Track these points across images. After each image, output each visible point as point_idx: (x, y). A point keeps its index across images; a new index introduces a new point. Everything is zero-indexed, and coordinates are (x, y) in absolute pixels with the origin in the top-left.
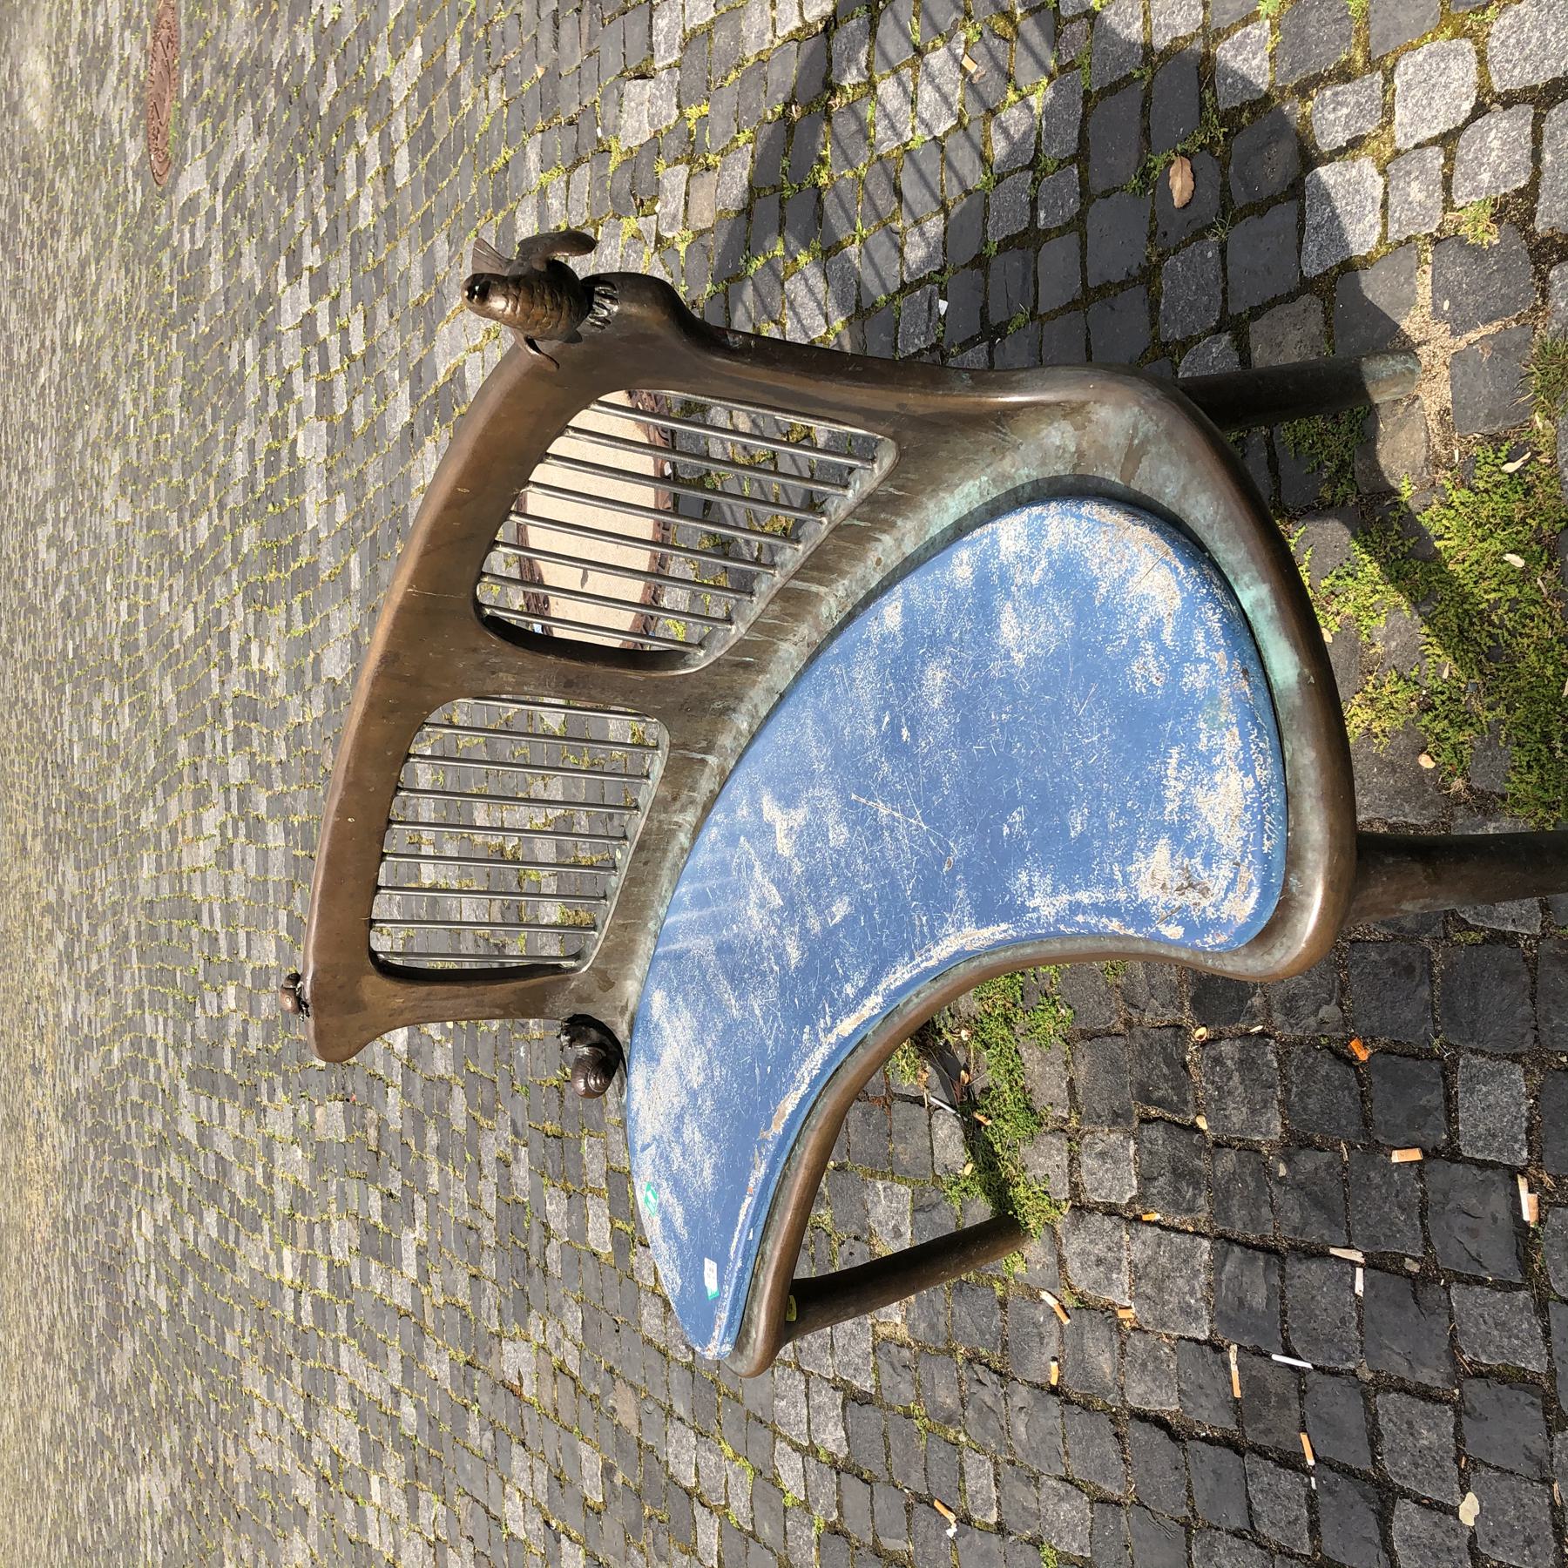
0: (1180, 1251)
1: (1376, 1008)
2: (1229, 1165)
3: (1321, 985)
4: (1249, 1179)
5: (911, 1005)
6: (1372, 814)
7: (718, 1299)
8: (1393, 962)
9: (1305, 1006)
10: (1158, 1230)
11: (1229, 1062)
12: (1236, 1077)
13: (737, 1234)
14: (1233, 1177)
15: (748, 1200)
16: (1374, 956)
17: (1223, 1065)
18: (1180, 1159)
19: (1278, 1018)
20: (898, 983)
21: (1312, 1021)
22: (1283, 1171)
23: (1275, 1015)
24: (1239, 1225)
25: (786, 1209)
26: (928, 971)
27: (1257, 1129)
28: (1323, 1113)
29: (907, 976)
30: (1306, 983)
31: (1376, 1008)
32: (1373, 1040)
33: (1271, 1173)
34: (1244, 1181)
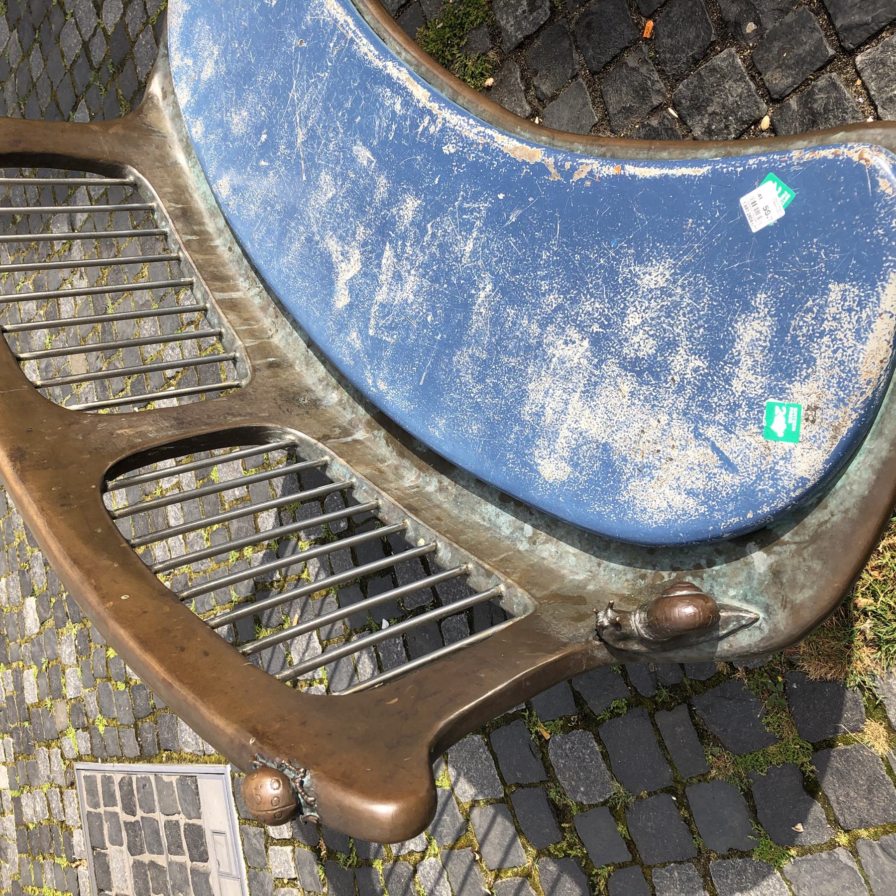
0: (880, 77)
1: (616, 31)
2: (777, 75)
3: (620, 77)
4: (775, 50)
5: (409, 57)
6: (524, 102)
7: (784, 176)
8: (588, 38)
9: (637, 79)
10: (880, 110)
11: (706, 122)
12: (710, 109)
13: (678, 172)
14: (783, 66)
15: (630, 169)
16: (591, 52)
17: (709, 125)
18: (802, 124)
19: (656, 100)
20: (372, 48)
21: (643, 70)
22: (751, 27)
23: (655, 103)
24: (816, 35)
25: (662, 163)
26: (358, 23)
27: (734, 66)
28: (693, 22)
29: (365, 41)
30: (624, 89)
31: (616, 31)
32: (638, 23)
33: (759, 32)
34: (780, 54)
